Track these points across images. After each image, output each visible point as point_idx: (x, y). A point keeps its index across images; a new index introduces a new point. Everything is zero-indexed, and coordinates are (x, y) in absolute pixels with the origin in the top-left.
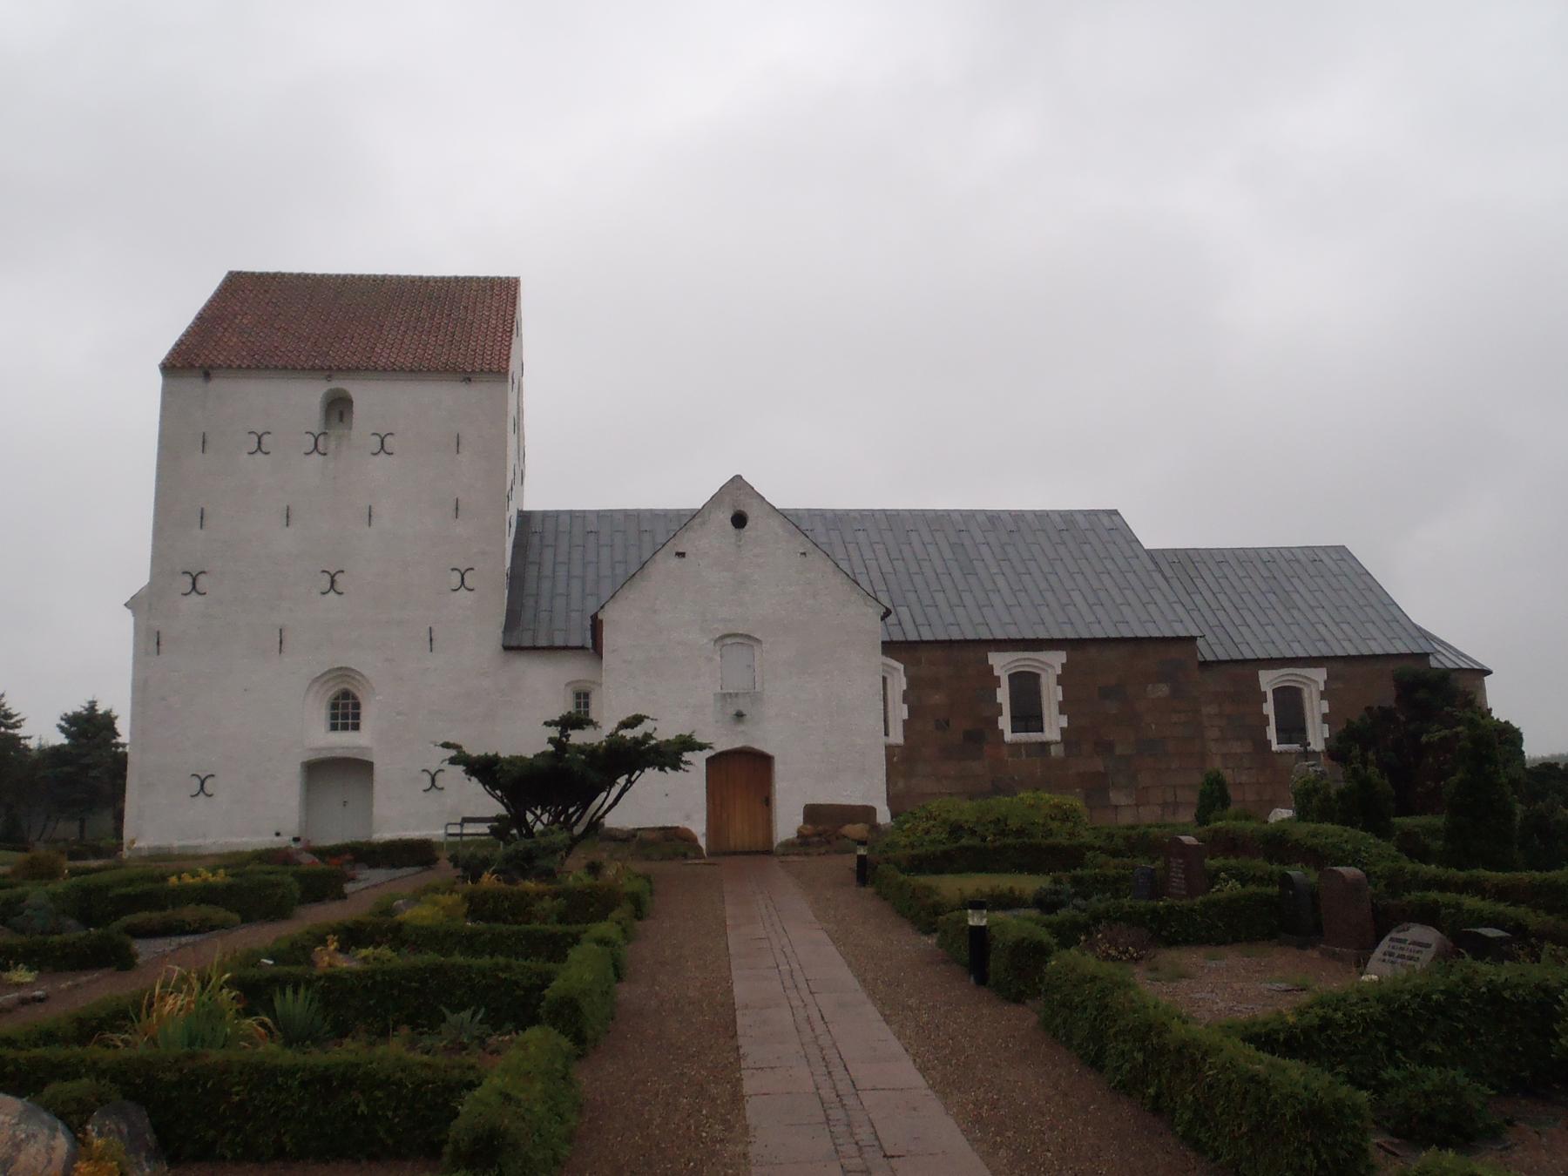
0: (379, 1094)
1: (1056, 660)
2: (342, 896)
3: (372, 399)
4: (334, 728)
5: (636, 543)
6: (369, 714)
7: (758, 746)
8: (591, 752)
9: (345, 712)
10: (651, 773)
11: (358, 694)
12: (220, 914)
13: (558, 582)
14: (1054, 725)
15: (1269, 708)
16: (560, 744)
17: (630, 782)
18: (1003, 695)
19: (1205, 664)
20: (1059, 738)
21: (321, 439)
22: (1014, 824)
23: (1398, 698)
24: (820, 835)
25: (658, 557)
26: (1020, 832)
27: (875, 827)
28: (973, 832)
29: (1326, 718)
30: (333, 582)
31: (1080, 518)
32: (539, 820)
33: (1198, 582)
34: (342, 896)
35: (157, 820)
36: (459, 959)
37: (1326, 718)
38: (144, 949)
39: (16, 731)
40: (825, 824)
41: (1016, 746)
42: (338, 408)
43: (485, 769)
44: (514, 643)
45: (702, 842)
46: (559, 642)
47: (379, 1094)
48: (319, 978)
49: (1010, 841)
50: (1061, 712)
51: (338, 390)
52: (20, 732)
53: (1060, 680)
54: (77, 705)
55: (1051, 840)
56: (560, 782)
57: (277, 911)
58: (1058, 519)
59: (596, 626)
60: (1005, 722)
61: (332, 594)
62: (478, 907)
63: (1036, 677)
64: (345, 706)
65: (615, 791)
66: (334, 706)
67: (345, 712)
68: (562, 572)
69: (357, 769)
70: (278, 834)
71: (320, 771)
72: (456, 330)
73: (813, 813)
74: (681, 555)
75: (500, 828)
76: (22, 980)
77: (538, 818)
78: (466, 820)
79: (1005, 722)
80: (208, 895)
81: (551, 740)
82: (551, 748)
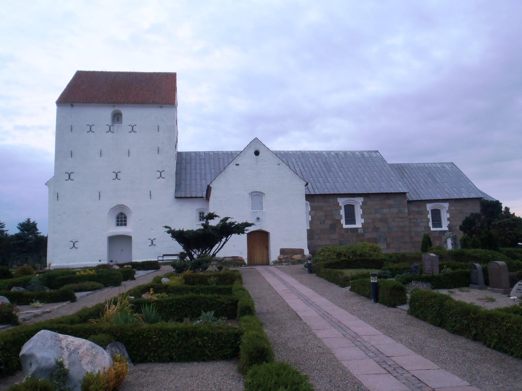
0: (206, 338)
1: (360, 201)
2: (133, 279)
3: (129, 114)
4: (118, 225)
5: (219, 162)
6: (130, 221)
7: (264, 229)
8: (214, 228)
9: (122, 219)
10: (234, 236)
11: (126, 214)
12: (98, 284)
13: (193, 175)
14: (359, 223)
15: (430, 216)
16: (206, 226)
17: (227, 240)
18: (342, 212)
19: (409, 202)
20: (361, 226)
21: (112, 127)
22: (359, 252)
23: (481, 211)
24: (285, 258)
25: (230, 165)
26: (361, 255)
27: (304, 256)
28: (345, 255)
29: (448, 219)
30: (117, 175)
31: (366, 154)
32: (196, 254)
33: (405, 174)
34: (133, 279)
35: (57, 258)
36: (202, 295)
37: (448, 219)
38: (78, 295)
39: (3, 229)
40: (288, 256)
41: (347, 229)
42: (117, 117)
43: (179, 236)
44: (179, 196)
45: (246, 261)
46: (194, 195)
47: (206, 338)
48: (153, 302)
49: (358, 258)
50: (362, 218)
51: (118, 110)
52: (4, 229)
53: (361, 207)
54: (23, 220)
55: (371, 258)
56: (200, 240)
57: (117, 284)
58: (358, 153)
59: (209, 189)
60: (343, 221)
61: (117, 179)
62: (187, 280)
63: (353, 206)
64: (121, 218)
65: (222, 243)
66: (118, 218)
67: (122, 219)
68: (193, 171)
69: (127, 239)
70: (100, 261)
71: (113, 240)
72: (156, 90)
73: (283, 251)
74: (237, 165)
75: (182, 256)
76: (38, 306)
77: (195, 253)
78: (164, 255)
79: (343, 221)
80: (91, 278)
81: (203, 225)
82: (202, 227)
